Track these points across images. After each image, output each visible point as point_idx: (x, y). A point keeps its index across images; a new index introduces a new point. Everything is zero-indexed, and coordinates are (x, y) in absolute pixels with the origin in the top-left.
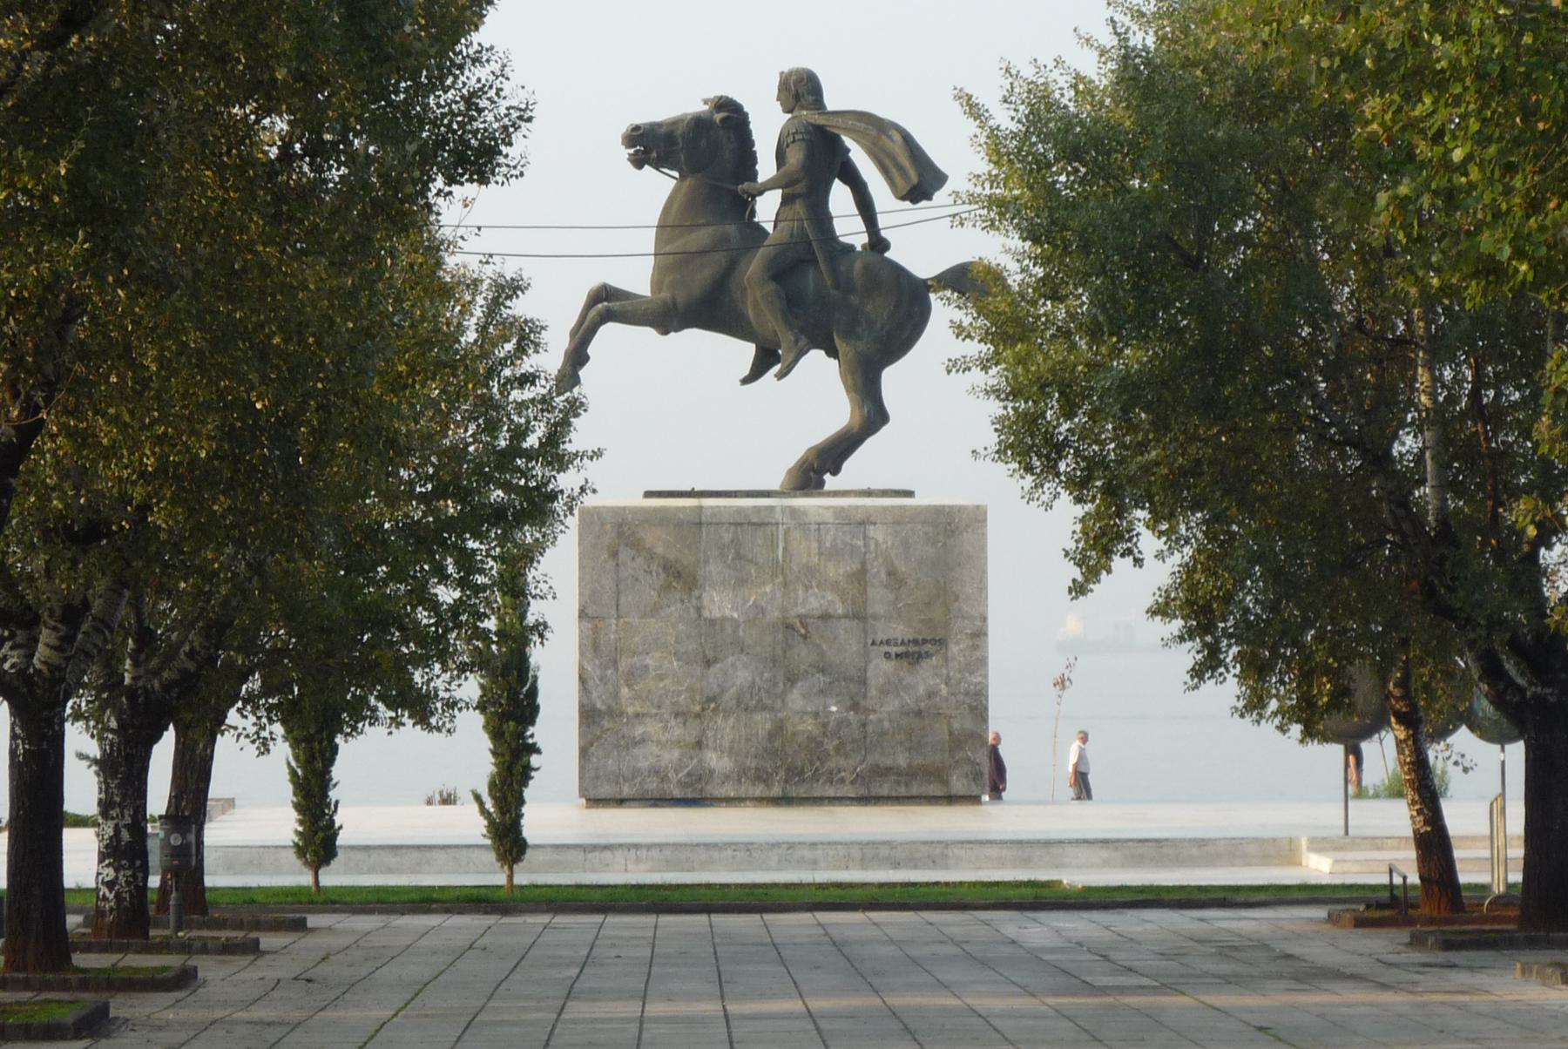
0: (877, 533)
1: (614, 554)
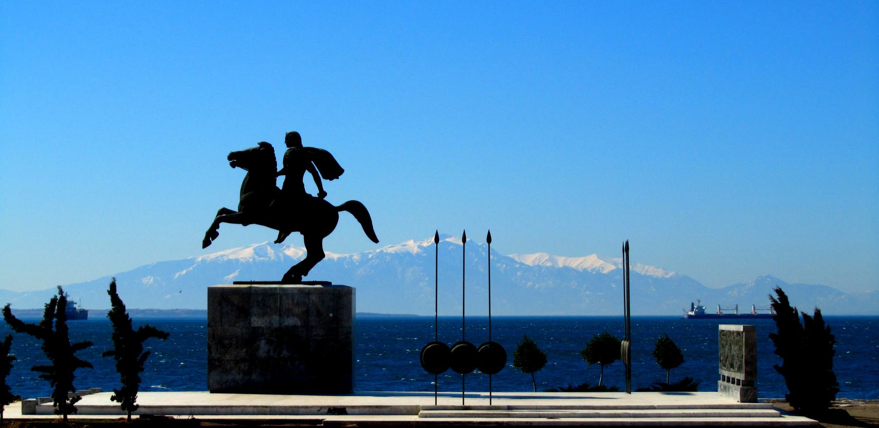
0: (313, 298)
1: (220, 304)
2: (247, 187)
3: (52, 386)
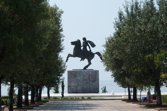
0: (91, 73)
1: (70, 74)
2: (75, 49)
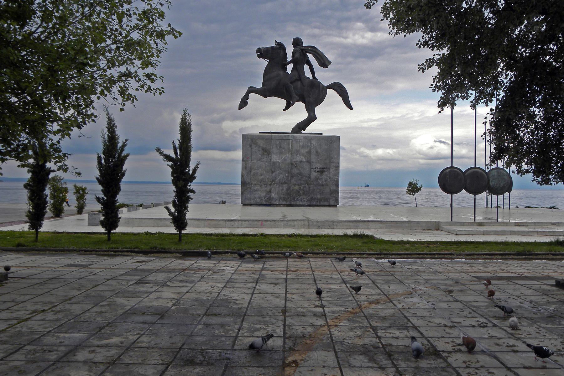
1: (251, 146)
3: (114, 124)
